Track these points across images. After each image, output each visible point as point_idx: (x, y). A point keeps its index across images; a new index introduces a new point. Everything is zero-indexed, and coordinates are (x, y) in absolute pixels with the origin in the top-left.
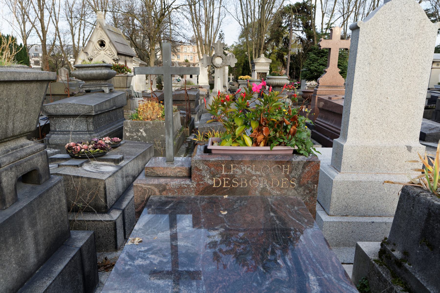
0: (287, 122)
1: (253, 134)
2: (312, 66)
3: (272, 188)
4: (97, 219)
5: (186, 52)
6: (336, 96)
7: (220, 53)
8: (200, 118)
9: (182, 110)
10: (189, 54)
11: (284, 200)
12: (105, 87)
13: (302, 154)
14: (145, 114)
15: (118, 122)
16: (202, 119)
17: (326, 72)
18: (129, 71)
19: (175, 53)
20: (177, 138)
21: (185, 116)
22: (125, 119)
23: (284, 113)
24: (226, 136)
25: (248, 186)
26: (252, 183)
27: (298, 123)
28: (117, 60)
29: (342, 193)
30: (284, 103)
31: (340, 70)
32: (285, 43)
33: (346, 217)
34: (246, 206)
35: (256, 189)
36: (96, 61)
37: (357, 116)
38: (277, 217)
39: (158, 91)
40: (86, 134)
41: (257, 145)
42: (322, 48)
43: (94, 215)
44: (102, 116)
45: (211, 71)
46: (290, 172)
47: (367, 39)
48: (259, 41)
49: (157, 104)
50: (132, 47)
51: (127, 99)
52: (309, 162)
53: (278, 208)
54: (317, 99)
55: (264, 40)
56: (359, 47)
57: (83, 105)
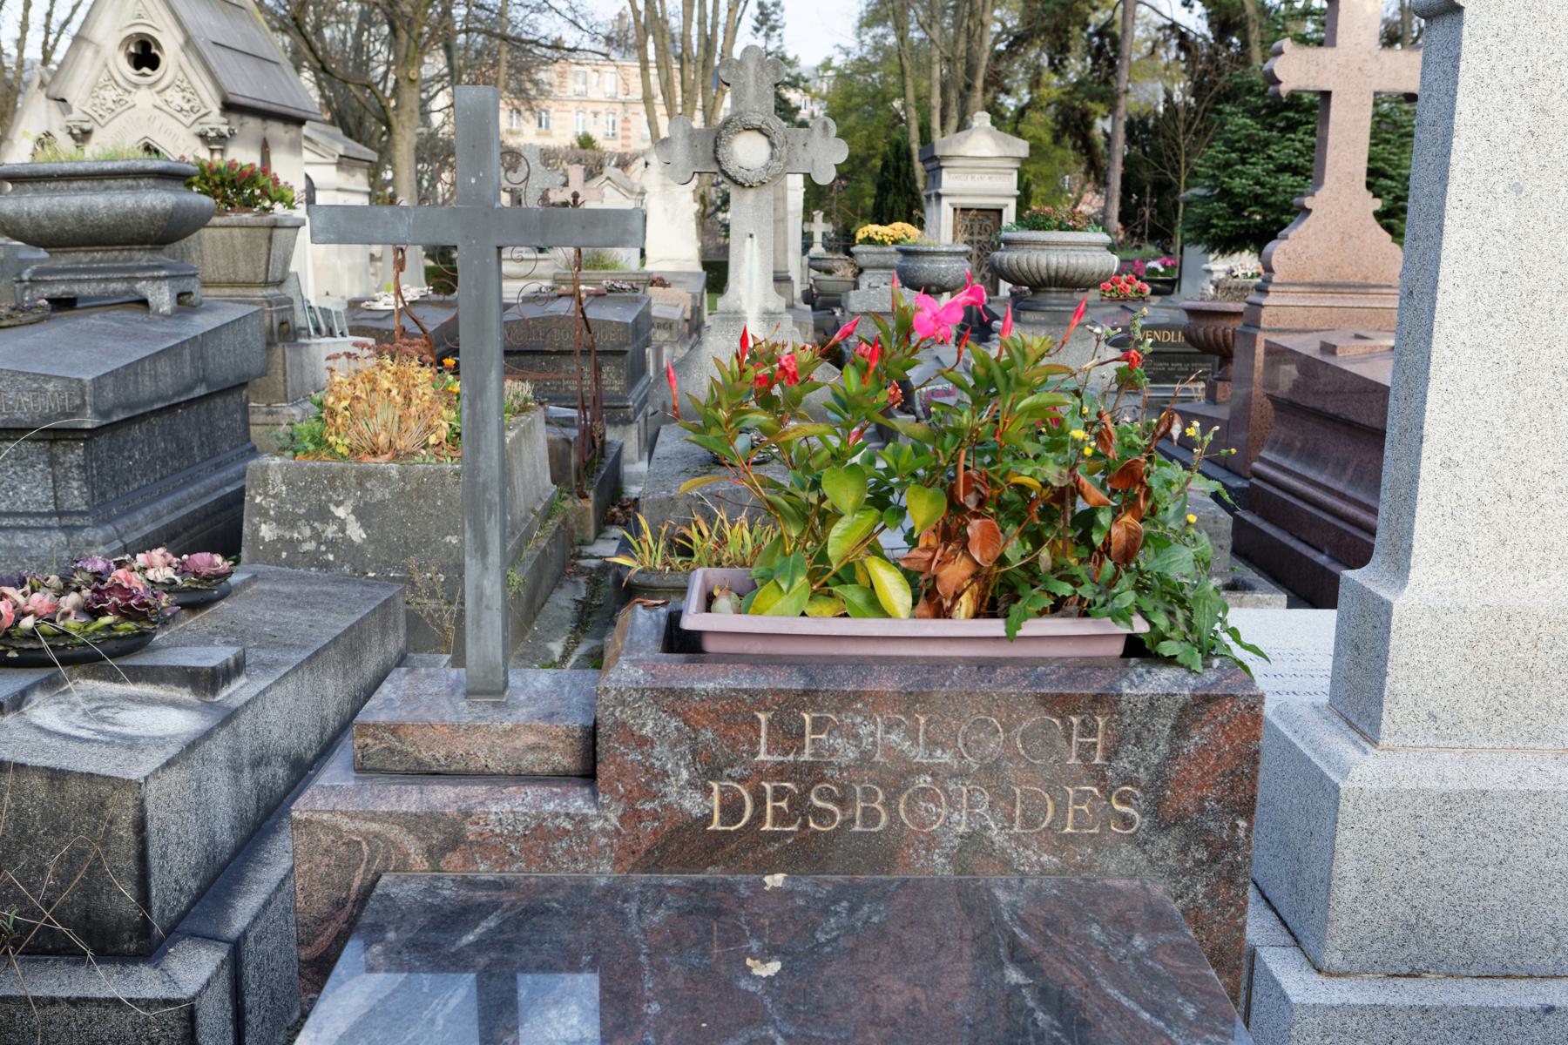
0: (1093, 492)
1: (915, 553)
2: (1240, 174)
3: (1017, 838)
4: (93, 991)
5: (582, 98)
6: (1358, 337)
7: (761, 110)
8: (650, 444)
9: (557, 400)
10: (601, 108)
11: (1085, 898)
12: (155, 279)
13: (1171, 661)
14: (362, 426)
15: (218, 466)
16: (660, 450)
17: (1308, 211)
18: (281, 201)
19: (528, 100)
20: (530, 552)
21: (573, 433)
22: (254, 452)
23: (1078, 445)
24: (777, 562)
25: (889, 827)
26: (910, 810)
27: (1147, 497)
28: (221, 138)
29: (1389, 853)
30: (1077, 393)
31: (1377, 204)
32: (1097, 54)
33: (1410, 984)
34: (881, 933)
35: (931, 842)
36: (109, 147)
37: (1458, 456)
38: (1044, 994)
39: (430, 303)
40: (48, 528)
41: (941, 613)
42: (1284, 89)
43: (82, 970)
44: (136, 431)
45: (713, 194)
46: (1111, 754)
47: (1500, 67)
48: (962, 46)
49: (427, 373)
50: (298, 69)
51: (270, 344)
52: (1208, 699)
53: (1047, 942)
54: (1260, 349)
55: (988, 42)
56: (1463, 104)
57: (35, 377)
